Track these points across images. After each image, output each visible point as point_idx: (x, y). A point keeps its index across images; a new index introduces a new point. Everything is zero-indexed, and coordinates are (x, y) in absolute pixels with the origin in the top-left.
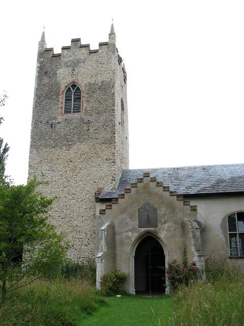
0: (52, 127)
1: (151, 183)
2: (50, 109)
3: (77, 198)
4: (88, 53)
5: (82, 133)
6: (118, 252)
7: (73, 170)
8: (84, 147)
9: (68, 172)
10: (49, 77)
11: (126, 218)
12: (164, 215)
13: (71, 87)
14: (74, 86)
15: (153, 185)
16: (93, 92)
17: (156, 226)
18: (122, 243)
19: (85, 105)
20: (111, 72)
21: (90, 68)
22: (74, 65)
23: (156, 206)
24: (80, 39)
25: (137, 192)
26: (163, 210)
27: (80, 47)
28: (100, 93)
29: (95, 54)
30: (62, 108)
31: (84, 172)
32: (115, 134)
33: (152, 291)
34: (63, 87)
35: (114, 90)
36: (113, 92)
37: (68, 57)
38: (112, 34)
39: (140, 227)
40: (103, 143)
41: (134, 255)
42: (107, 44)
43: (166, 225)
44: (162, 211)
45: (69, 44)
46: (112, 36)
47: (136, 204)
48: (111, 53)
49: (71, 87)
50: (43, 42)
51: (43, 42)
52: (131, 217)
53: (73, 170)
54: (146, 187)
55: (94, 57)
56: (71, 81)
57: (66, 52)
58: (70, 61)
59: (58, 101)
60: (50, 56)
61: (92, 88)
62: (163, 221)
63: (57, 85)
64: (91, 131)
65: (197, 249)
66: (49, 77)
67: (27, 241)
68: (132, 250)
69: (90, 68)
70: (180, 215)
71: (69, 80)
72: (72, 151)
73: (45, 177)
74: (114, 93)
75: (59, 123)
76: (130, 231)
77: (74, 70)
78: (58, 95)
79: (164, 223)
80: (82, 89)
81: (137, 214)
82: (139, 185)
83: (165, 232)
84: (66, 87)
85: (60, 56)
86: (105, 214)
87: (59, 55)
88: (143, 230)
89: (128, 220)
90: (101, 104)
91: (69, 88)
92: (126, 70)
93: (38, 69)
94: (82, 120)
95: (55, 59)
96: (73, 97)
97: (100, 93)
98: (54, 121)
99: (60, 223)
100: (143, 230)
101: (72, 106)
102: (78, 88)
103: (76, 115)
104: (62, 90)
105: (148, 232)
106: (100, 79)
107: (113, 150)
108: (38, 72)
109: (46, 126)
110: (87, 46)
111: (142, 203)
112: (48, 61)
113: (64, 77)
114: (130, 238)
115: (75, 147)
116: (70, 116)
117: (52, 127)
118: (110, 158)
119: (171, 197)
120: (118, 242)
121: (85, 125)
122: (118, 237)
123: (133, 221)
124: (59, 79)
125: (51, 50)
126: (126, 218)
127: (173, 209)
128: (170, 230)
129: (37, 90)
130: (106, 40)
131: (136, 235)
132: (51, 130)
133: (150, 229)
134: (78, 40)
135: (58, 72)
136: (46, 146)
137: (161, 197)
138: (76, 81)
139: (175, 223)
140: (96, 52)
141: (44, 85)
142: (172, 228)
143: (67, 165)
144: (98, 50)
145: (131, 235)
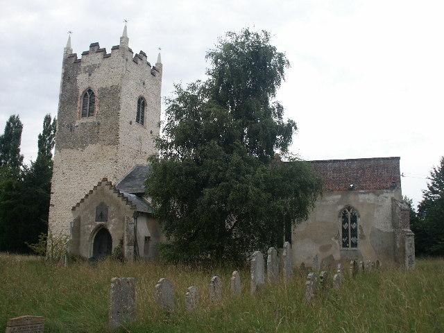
5: (93, 135)
6: (81, 239)
14: (90, 90)
15: (107, 188)
19: (97, 109)
22: (91, 70)
26: (112, 208)
33: (272, 55)
34: (81, 92)
37: (89, 61)
39: (97, 221)
41: (93, 242)
44: (112, 209)
45: (88, 49)
54: (102, 189)
55: (107, 61)
61: (103, 91)
63: (76, 90)
64: (101, 134)
67: (157, 160)
68: (91, 238)
77: (90, 75)
78: (77, 100)
80: (96, 94)
88: (98, 223)
100: (98, 223)
105: (101, 225)
108: (63, 78)
110: (104, 50)
113: (82, 82)
114: (88, 229)
122: (82, 228)
125: (75, 55)
130: (117, 43)
131: (94, 227)
134: (97, 44)
135: (77, 78)
137: (111, 197)
145: (90, 227)
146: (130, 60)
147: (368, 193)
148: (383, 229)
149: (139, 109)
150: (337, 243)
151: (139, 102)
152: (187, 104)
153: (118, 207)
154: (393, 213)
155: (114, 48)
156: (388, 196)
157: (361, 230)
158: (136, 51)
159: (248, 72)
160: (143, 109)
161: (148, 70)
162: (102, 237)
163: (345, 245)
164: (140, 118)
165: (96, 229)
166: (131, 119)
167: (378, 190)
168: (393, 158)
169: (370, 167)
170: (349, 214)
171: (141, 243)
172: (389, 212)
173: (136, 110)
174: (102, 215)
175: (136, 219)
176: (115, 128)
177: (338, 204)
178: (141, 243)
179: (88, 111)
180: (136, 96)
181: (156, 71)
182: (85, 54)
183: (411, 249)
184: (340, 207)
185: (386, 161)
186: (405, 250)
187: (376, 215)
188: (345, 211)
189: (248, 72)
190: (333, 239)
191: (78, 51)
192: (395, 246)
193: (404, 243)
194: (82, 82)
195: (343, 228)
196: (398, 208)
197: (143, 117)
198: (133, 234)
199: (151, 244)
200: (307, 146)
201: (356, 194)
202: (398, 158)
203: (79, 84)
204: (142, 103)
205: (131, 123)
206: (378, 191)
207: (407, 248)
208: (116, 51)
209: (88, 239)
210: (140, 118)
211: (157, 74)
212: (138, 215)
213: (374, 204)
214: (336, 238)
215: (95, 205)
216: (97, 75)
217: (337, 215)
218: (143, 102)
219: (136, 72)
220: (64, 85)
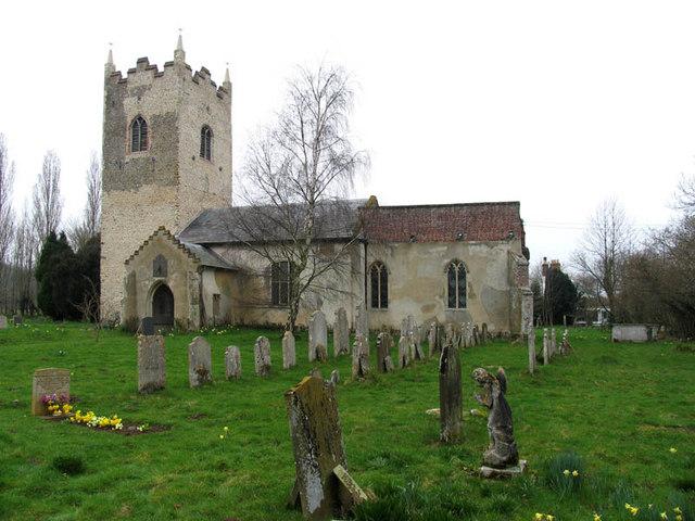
5: (147, 174)
14: (140, 119)
15: (165, 238)
17: (166, 276)
22: (140, 92)
34: (129, 120)
38: (180, 53)
43: (174, 276)
44: (171, 262)
45: (134, 66)
50: (110, 65)
57: (131, 76)
77: (139, 99)
80: (148, 122)
87: (125, 81)
88: (157, 279)
100: (157, 279)
112: (115, 84)
113: (131, 107)
114: (146, 286)
122: (138, 285)
129: (105, 124)
135: (124, 102)
145: (147, 283)
147: (480, 245)
150: (444, 302)
151: (203, 132)
155: (168, 65)
156: (503, 248)
158: (196, 68)
160: (209, 140)
162: (163, 295)
163: (451, 305)
164: (206, 152)
168: (511, 204)
170: (457, 269)
173: (198, 141)
174: (160, 269)
176: (174, 165)
179: (140, 143)
181: (224, 93)
182: (131, 72)
184: (446, 261)
190: (437, 298)
191: (124, 66)
193: (520, 303)
194: (131, 107)
204: (207, 133)
205: (194, 159)
207: (523, 310)
210: (206, 152)
211: (226, 96)
216: (148, 98)
217: (442, 270)
220: (107, 112)
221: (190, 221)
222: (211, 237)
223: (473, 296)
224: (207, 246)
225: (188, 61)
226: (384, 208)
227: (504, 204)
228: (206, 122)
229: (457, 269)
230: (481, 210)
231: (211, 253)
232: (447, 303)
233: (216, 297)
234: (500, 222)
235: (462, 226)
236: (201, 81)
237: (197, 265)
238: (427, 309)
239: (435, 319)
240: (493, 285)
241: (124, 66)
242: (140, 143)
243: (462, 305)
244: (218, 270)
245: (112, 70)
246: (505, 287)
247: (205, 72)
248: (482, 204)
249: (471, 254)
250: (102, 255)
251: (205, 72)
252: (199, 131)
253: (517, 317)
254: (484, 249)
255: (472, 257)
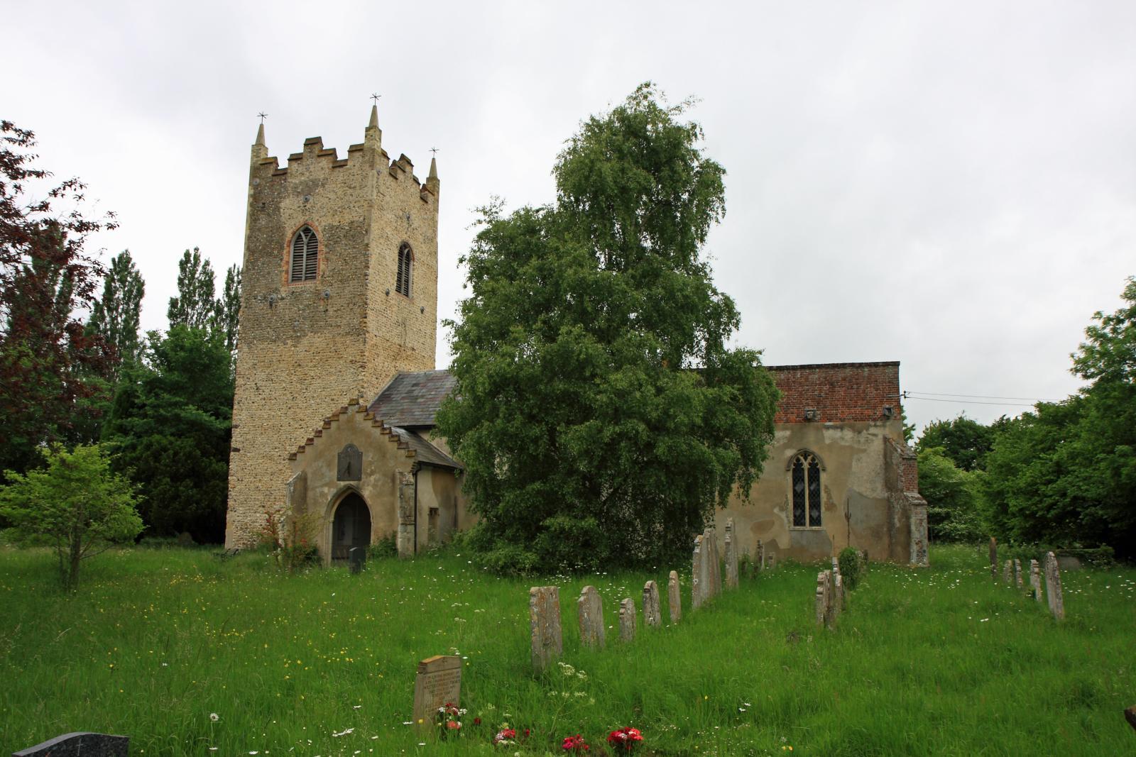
0: (271, 305)
1: (357, 415)
2: (269, 273)
3: (305, 426)
4: (331, 165)
7: (301, 381)
8: (318, 341)
9: (294, 383)
10: (268, 214)
11: (322, 467)
12: (371, 463)
13: (302, 234)
14: (307, 230)
15: (360, 417)
16: (336, 242)
17: (359, 479)
18: (316, 503)
20: (366, 204)
21: (332, 196)
22: (308, 190)
23: (361, 450)
24: (320, 138)
25: (339, 428)
27: (319, 156)
28: (346, 245)
29: (341, 169)
30: (287, 272)
31: (317, 383)
32: (366, 318)
34: (289, 234)
35: (369, 239)
36: (366, 242)
38: (373, 129)
39: (339, 480)
40: (348, 334)
41: (332, 519)
42: (361, 150)
43: (372, 478)
44: (368, 457)
45: (300, 149)
46: (371, 132)
47: (336, 446)
48: (367, 167)
49: (302, 234)
50: (259, 145)
51: (259, 145)
52: (329, 465)
53: (301, 381)
54: (350, 420)
55: (340, 175)
56: (302, 223)
57: (295, 165)
58: (301, 183)
59: (281, 260)
60: (270, 175)
62: (369, 471)
63: (280, 228)
64: (331, 313)
65: (405, 513)
66: (268, 214)
68: (328, 512)
69: (332, 196)
70: (392, 463)
71: (299, 220)
72: (301, 348)
73: (261, 392)
74: (367, 245)
75: (282, 299)
76: (326, 485)
77: (307, 200)
78: (282, 248)
79: (370, 476)
80: (319, 236)
81: (336, 461)
82: (342, 417)
83: (370, 488)
84: (294, 234)
85: (286, 173)
86: (295, 460)
87: (284, 172)
88: (342, 484)
89: (324, 469)
90: (347, 263)
91: (300, 235)
92: (636, 89)
93: (251, 200)
94: (317, 293)
95: (277, 179)
96: (305, 251)
97: (346, 245)
98: (274, 296)
99: (280, 467)
101: (304, 267)
102: (313, 234)
103: (309, 285)
104: (287, 239)
105: (349, 488)
106: (348, 218)
107: (361, 347)
108: (251, 205)
109: (262, 305)
110: (332, 153)
111: (344, 444)
112: (266, 177)
113: (291, 214)
114: (323, 495)
115: (305, 341)
116: (299, 286)
117: (271, 305)
118: (357, 360)
119: (382, 436)
120: (310, 501)
121: (322, 303)
122: (310, 494)
123: (330, 471)
124: (283, 219)
126: (322, 467)
127: (382, 452)
128: (377, 486)
129: (249, 239)
130: (360, 139)
131: (334, 491)
132: (269, 311)
133: (352, 483)
135: (282, 205)
136: (262, 339)
138: (310, 222)
139: (385, 475)
140: (343, 164)
141: (259, 230)
142: (380, 483)
143: (293, 372)
144: (346, 160)
145: (327, 490)
146: (385, 172)
147: (842, 428)
148: (868, 493)
149: (400, 267)
150: (787, 516)
151: (401, 254)
152: (512, 248)
153: (382, 452)
154: (887, 465)
155: (354, 150)
156: (879, 432)
157: (828, 492)
158: (394, 156)
159: (641, 180)
160: (408, 265)
161: (415, 190)
162: (351, 510)
163: (799, 521)
164: (403, 285)
165: (337, 496)
166: (387, 286)
167: (858, 422)
168: (886, 364)
169: (844, 379)
170: (806, 465)
171: (424, 520)
172: (881, 462)
173: (395, 268)
174: (350, 466)
175: (415, 475)
176: (360, 303)
177: (786, 446)
178: (424, 520)
179: (305, 269)
180: (397, 242)
181: (429, 191)
182: (294, 158)
183: (922, 529)
184: (790, 453)
185: (873, 369)
186: (909, 532)
187: (855, 467)
188: (798, 460)
189: (641, 180)
190: (776, 510)
191: (282, 149)
192: (891, 525)
193: (908, 518)
194: (291, 214)
195: (794, 491)
196: (896, 455)
197: (407, 281)
198: (412, 504)
199: (439, 521)
200: (774, 328)
201: (818, 429)
202: (896, 364)
203: (284, 216)
204: (405, 254)
205: (387, 294)
206: (859, 424)
207: (913, 528)
208: (358, 154)
209: (323, 513)
210: (403, 285)
211: (430, 198)
212: (419, 467)
213: (851, 447)
214: (782, 509)
215: (336, 450)
216: (321, 200)
217: (783, 466)
218: (408, 254)
219: (395, 196)
220: (253, 217)
221: (380, 391)
222: (419, 418)
223: (831, 507)
224: (414, 430)
225: (386, 145)
226: (771, 368)
227: (876, 365)
228: (405, 237)
229: (806, 465)
230: (841, 374)
231: (420, 440)
232: (792, 519)
233: (433, 512)
234: (872, 392)
235: (813, 399)
236: (400, 176)
237: (411, 461)
238: (760, 527)
239: (773, 544)
240: (862, 490)
241: (282, 149)
242: (305, 269)
243: (816, 521)
244: (61, 559)
245: (263, 156)
246: (881, 493)
247: (404, 162)
248: (843, 366)
249: (827, 442)
250: (233, 445)
251: (404, 162)
252: (397, 252)
253: (902, 538)
254: (848, 434)
255: (830, 446)
